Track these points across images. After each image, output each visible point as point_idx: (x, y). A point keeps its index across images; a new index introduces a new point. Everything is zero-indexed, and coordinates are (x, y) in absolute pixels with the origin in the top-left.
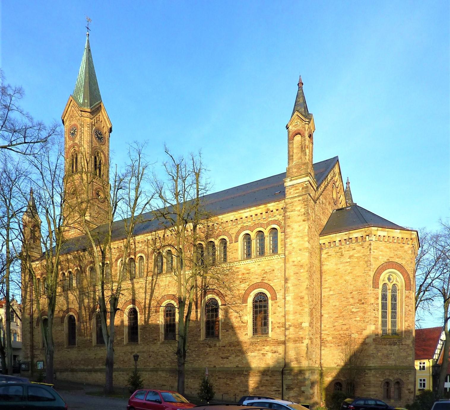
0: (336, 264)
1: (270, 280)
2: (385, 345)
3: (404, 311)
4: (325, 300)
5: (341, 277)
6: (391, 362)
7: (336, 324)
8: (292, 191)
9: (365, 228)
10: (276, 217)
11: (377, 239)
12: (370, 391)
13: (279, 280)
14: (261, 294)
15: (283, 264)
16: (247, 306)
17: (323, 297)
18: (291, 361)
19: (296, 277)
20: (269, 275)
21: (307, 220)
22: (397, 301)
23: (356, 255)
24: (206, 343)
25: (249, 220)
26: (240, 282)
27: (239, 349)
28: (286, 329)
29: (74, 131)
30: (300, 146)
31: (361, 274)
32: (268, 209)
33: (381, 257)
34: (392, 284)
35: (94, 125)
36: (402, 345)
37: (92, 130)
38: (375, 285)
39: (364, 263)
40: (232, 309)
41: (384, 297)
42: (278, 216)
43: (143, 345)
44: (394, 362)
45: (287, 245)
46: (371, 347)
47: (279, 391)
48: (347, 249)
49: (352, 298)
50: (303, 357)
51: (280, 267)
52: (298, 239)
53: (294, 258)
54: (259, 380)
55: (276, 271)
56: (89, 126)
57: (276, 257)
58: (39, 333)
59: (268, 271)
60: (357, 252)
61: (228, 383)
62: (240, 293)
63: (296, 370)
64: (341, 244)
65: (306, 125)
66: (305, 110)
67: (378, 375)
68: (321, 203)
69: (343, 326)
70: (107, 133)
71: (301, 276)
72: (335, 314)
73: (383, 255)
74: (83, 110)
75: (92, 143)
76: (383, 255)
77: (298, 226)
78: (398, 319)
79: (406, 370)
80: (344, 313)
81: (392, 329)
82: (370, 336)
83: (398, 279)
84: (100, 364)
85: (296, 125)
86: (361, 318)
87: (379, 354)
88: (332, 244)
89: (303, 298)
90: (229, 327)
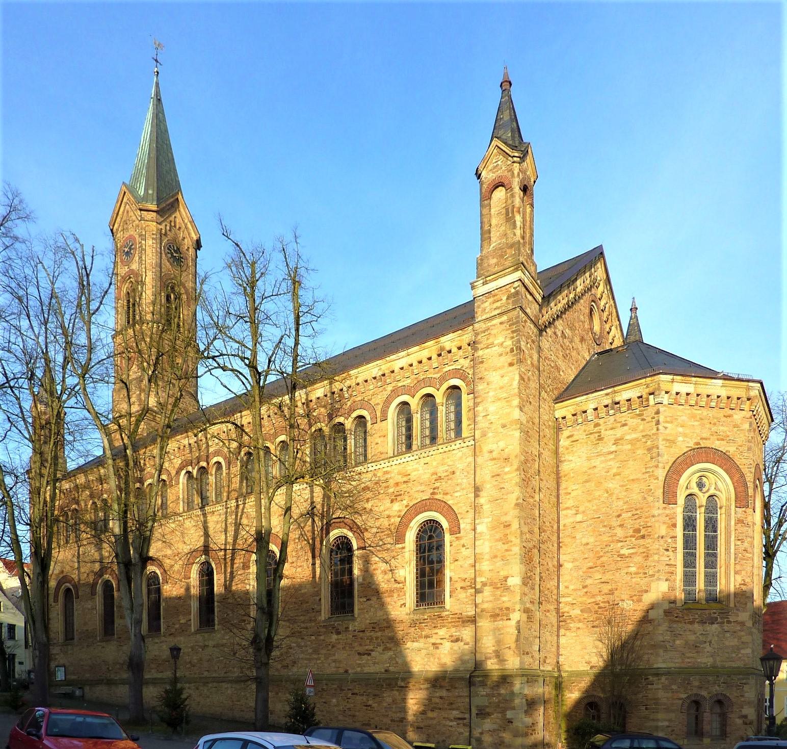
0: (589, 459)
1: (447, 494)
2: (692, 623)
3: (732, 550)
4: (567, 533)
5: (599, 484)
6: (704, 660)
7: (589, 582)
8: (487, 304)
9: (645, 377)
11: (672, 401)
12: (658, 720)
13: (465, 492)
14: (430, 523)
15: (471, 459)
16: (403, 548)
17: (561, 528)
18: (487, 658)
19: (496, 483)
21: (517, 363)
22: (719, 532)
23: (628, 437)
24: (331, 625)
25: (407, 375)
26: (392, 501)
27: (390, 635)
28: (478, 591)
29: (130, 249)
30: (504, 211)
31: (640, 476)
32: (442, 349)
33: (681, 439)
34: (707, 495)
35: (166, 234)
36: (729, 622)
37: (161, 244)
38: (669, 497)
39: (646, 452)
40: (376, 556)
41: (690, 524)
42: (462, 361)
43: (222, 632)
44: (711, 660)
45: (479, 419)
46: (660, 628)
47: (465, 719)
48: (611, 426)
49: (621, 526)
50: (509, 648)
51: (466, 464)
52: (499, 404)
53: (491, 444)
54: (426, 697)
55: (458, 473)
56: (155, 236)
57: (458, 446)
58: (58, 614)
59: (443, 475)
60: (630, 431)
61: (370, 703)
62: (391, 523)
63: (495, 676)
64: (598, 417)
65: (515, 164)
66: (513, 137)
67: (674, 687)
68: (559, 334)
69: (602, 585)
70: (192, 251)
71: (506, 480)
72: (586, 561)
73: (685, 435)
74: (144, 208)
75: (161, 268)
76: (685, 435)
77: (498, 377)
78: (720, 568)
79: (738, 677)
80: (604, 559)
81: (706, 590)
82: (658, 604)
83: (720, 484)
84: (153, 671)
85: (495, 167)
86: (638, 568)
87: (678, 642)
88: (579, 417)
89: (509, 525)
90: (373, 592)
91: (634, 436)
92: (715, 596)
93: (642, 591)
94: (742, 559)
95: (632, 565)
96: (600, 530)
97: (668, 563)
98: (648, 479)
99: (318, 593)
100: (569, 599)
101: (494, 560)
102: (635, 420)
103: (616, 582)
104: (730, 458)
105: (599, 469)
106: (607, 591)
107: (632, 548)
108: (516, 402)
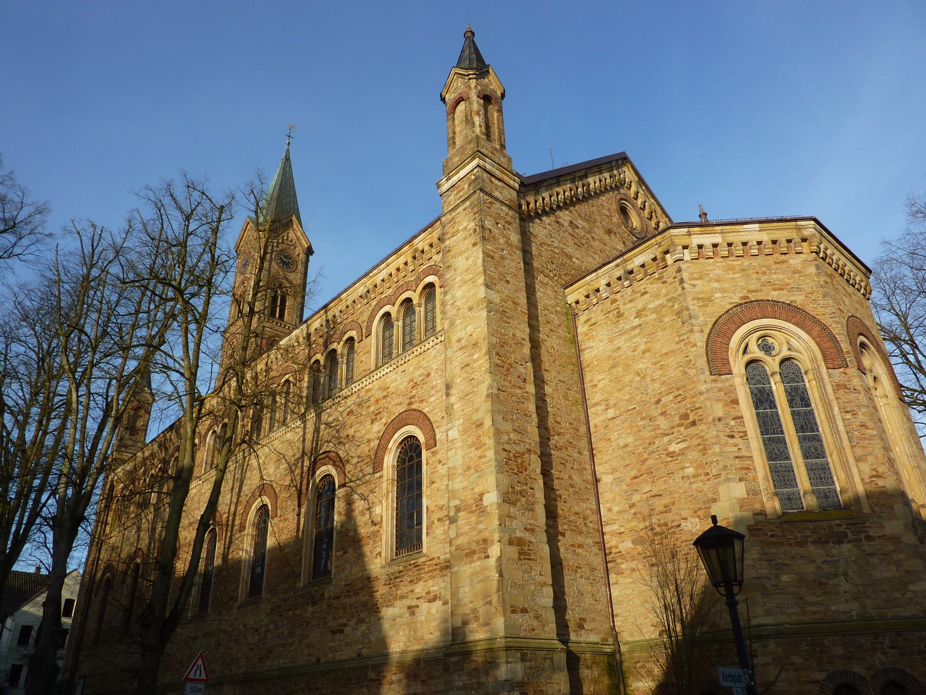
0: (611, 341)
1: (421, 401)
2: (802, 544)
3: (841, 427)
5: (627, 367)
7: (636, 498)
8: (452, 197)
10: (431, 260)
16: (381, 477)
17: (592, 430)
20: (422, 388)
23: (651, 306)
26: (372, 422)
31: (674, 347)
32: (416, 250)
33: (718, 295)
34: (778, 359)
41: (763, 399)
44: (855, 606)
49: (663, 414)
52: (465, 287)
57: (431, 344)
60: (652, 298)
67: (796, 659)
69: (654, 499)
72: (628, 468)
73: (723, 291)
76: (723, 291)
78: (831, 455)
80: (650, 462)
83: (794, 342)
86: (696, 468)
87: (785, 578)
88: (592, 297)
91: (657, 303)
92: (835, 499)
93: (708, 501)
94: (861, 439)
95: (687, 465)
96: (639, 424)
97: (737, 454)
98: (684, 348)
99: (299, 552)
100: (614, 527)
101: (468, 473)
102: (655, 285)
103: (671, 493)
104: (798, 308)
105: (624, 349)
106: (662, 509)
107: (683, 441)
108: (481, 280)
